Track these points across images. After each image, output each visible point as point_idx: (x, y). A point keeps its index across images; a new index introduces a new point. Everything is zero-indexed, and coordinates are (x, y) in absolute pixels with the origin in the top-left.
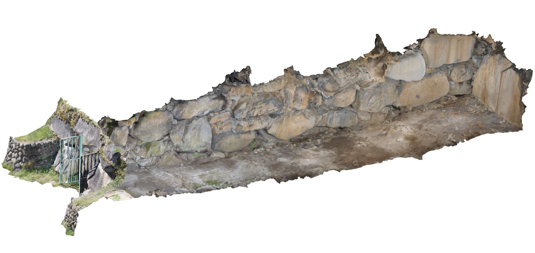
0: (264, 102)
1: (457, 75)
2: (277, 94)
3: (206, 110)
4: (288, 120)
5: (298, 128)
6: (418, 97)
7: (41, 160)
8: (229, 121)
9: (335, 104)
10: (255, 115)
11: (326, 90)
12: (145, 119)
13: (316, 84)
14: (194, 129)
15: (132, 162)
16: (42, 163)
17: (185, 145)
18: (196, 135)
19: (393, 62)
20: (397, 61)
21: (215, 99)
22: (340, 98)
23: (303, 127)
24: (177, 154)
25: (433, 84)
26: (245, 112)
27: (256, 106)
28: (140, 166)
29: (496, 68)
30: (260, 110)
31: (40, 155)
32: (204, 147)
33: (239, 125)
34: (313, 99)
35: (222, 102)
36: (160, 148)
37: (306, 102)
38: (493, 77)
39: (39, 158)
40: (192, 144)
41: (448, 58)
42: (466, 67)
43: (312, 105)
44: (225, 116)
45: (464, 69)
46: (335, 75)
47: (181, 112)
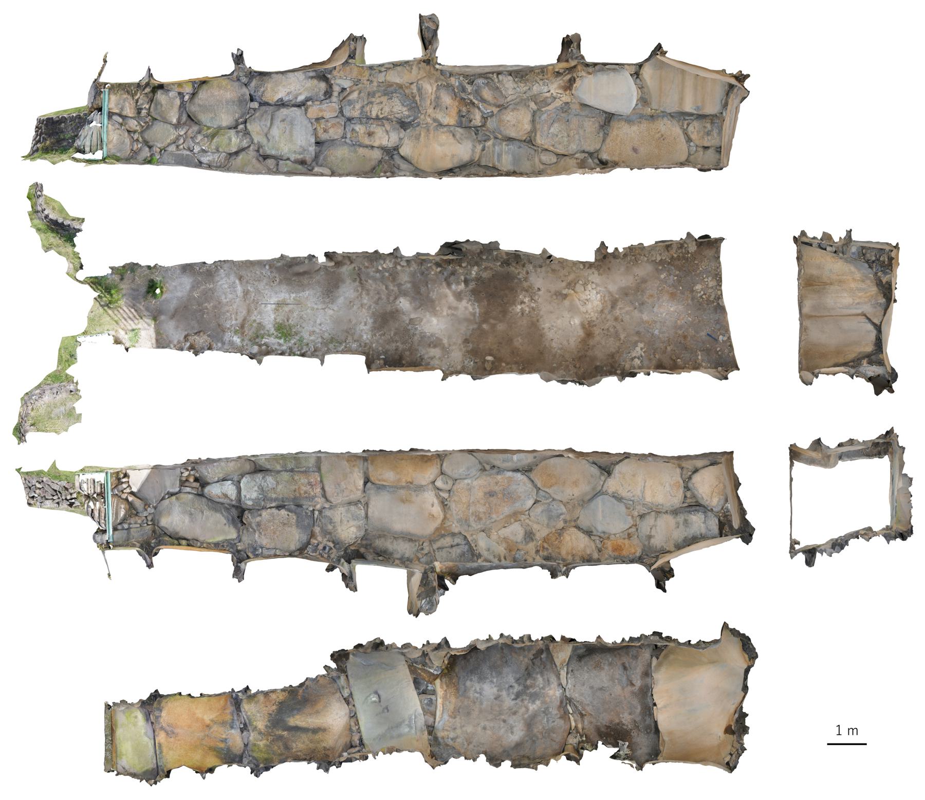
0: (385, 95)
1: (698, 132)
2: (407, 87)
3: (300, 94)
4: (427, 136)
5: (446, 155)
6: (635, 150)
7: (64, 139)
8: (338, 120)
9: (502, 129)
10: (374, 115)
11: (483, 101)
12: (205, 87)
13: (469, 88)
14: (283, 120)
15: (188, 153)
16: (65, 144)
17: (270, 144)
18: (287, 131)
19: (583, 74)
20: (589, 73)
21: (312, 78)
22: (508, 118)
23: (453, 156)
24: (261, 159)
25: (659, 135)
26: (358, 106)
27: (373, 100)
28: (201, 163)
29: (865, 303)
30: (380, 107)
31: (62, 132)
32: (300, 154)
33: (353, 130)
34: (464, 109)
35: (323, 85)
36: (230, 140)
37: (454, 112)
38: (851, 300)
39: (62, 137)
40: (282, 145)
41: (682, 99)
42: (712, 123)
43: (464, 122)
44: (329, 109)
45: (708, 126)
46: (499, 81)
47: (262, 89)
